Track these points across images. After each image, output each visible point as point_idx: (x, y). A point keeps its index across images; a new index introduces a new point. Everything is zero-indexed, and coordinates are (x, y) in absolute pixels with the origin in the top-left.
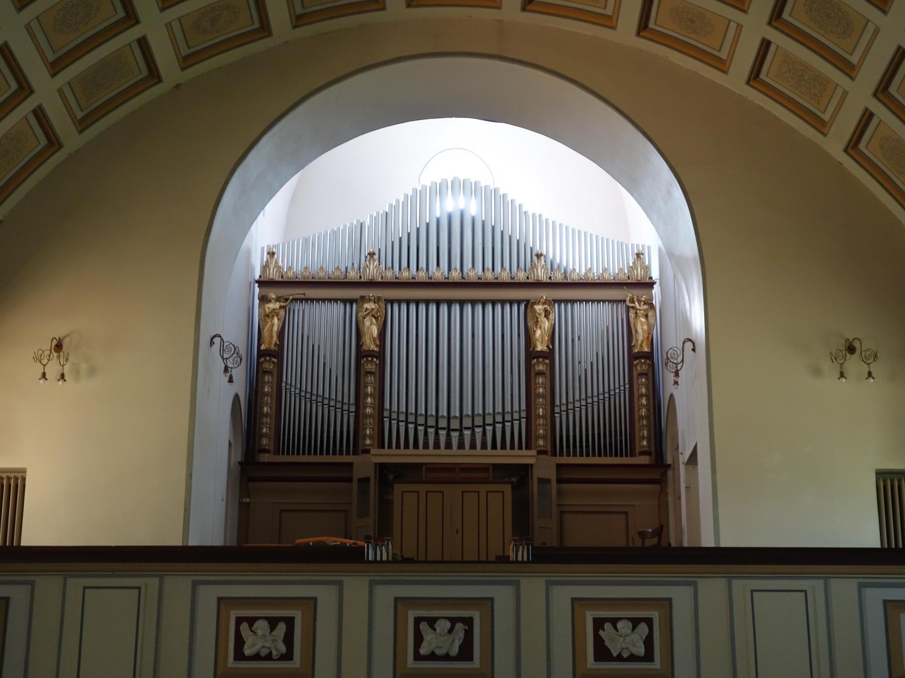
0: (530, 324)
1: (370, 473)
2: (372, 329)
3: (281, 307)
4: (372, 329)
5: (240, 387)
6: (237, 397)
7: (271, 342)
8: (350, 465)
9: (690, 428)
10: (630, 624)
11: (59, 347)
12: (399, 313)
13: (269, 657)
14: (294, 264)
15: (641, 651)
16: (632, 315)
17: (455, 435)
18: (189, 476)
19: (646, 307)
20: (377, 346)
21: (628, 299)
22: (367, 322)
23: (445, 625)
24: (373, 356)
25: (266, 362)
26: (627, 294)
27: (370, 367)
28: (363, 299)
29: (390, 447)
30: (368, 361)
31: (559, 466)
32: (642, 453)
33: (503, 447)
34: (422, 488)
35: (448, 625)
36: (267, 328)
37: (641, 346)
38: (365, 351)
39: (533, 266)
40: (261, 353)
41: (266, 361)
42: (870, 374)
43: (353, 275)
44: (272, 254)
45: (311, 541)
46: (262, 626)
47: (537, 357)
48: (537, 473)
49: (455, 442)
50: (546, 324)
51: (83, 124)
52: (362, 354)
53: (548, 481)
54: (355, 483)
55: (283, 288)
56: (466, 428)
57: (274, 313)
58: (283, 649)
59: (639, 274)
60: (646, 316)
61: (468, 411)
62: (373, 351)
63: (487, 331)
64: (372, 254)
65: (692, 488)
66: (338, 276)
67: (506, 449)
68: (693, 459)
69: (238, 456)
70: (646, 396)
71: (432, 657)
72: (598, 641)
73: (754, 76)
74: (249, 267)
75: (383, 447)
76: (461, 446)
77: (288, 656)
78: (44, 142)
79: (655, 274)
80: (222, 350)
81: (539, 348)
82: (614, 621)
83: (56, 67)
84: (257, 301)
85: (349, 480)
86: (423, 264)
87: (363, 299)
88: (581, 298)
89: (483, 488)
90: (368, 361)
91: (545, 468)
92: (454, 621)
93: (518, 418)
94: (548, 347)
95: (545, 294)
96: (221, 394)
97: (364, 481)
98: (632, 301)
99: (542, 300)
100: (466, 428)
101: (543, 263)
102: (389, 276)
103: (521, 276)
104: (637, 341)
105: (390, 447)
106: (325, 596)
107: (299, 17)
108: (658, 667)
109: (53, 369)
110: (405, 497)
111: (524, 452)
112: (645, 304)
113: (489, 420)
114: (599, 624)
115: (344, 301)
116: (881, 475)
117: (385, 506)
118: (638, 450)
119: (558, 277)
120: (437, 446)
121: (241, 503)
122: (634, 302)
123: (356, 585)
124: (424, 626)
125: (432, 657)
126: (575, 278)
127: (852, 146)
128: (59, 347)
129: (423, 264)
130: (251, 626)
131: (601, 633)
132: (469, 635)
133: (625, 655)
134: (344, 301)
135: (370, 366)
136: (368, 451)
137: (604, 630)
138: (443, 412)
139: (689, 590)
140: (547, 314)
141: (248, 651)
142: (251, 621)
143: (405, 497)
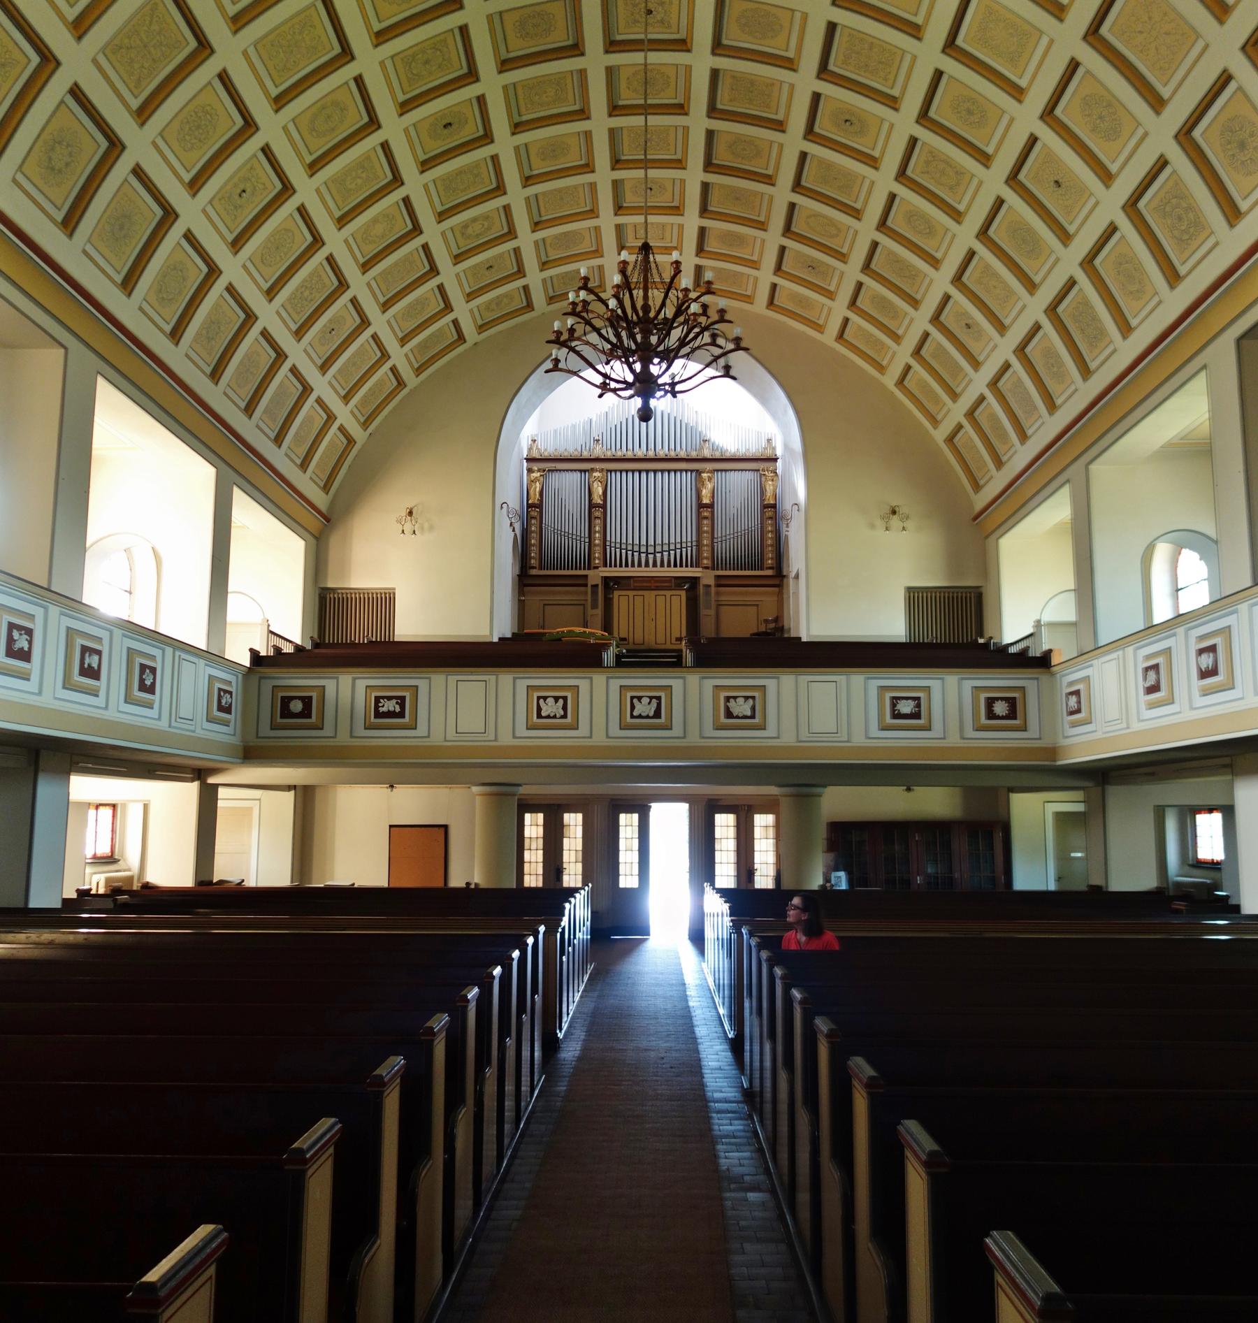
1: (599, 582)
7: (534, 499)
8: (586, 576)
9: (796, 561)
11: (410, 513)
12: (615, 478)
13: (555, 717)
14: (548, 447)
15: (749, 713)
17: (651, 557)
18: (492, 592)
22: (595, 485)
25: (533, 510)
26: (761, 466)
27: (597, 514)
28: (593, 470)
30: (596, 510)
31: (718, 577)
34: (631, 593)
40: (529, 506)
43: (586, 454)
45: (565, 629)
46: (550, 700)
48: (704, 581)
50: (709, 486)
51: (419, 371)
52: (592, 506)
55: (543, 463)
59: (769, 453)
61: (659, 541)
63: (678, 485)
65: (796, 594)
68: (797, 577)
71: (640, 716)
73: (841, 336)
74: (521, 449)
77: (565, 716)
78: (395, 383)
79: (779, 453)
85: (586, 585)
86: (630, 446)
87: (593, 470)
89: (668, 593)
90: (596, 510)
92: (651, 698)
102: (609, 454)
103: (694, 455)
106: (583, 685)
107: (551, 298)
109: (408, 527)
110: (621, 599)
113: (672, 547)
114: (728, 699)
115: (581, 471)
116: (910, 590)
117: (608, 603)
119: (718, 455)
121: (520, 601)
123: (599, 678)
124: (635, 701)
125: (640, 716)
126: (728, 455)
127: (901, 382)
128: (410, 513)
129: (630, 446)
134: (581, 471)
138: (644, 542)
140: (710, 479)
141: (543, 714)
142: (545, 698)
143: (621, 599)
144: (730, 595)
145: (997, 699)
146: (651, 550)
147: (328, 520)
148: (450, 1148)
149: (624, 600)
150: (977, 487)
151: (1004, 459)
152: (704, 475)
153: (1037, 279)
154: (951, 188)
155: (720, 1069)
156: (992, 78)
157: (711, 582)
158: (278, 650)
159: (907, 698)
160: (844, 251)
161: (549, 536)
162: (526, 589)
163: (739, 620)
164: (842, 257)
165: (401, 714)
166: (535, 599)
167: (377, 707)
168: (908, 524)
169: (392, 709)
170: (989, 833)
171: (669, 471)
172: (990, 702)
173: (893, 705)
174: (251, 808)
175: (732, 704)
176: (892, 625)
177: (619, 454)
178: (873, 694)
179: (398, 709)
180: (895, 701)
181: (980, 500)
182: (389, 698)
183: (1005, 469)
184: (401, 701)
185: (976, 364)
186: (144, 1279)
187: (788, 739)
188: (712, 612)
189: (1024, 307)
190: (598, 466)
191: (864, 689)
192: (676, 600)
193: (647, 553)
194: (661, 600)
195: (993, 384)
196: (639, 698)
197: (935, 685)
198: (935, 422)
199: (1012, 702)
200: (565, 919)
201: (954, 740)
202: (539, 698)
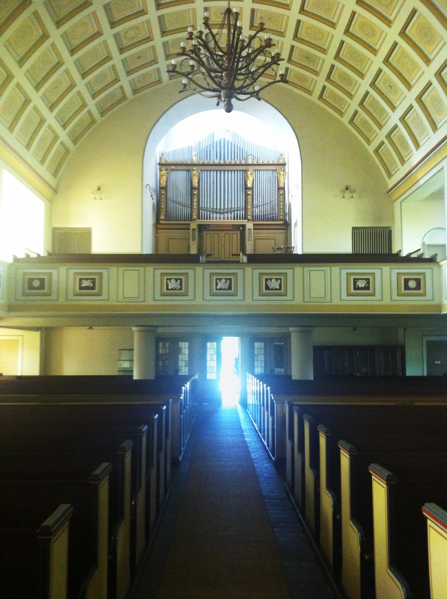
4: (195, 181)
5: (155, 201)
6: (154, 203)
8: (189, 224)
10: (275, 280)
11: (99, 189)
12: (204, 174)
13: (175, 289)
15: (278, 287)
16: (279, 175)
23: (223, 281)
25: (162, 192)
30: (193, 190)
33: (237, 219)
35: (225, 280)
39: (247, 159)
42: (352, 197)
44: (162, 155)
52: (192, 188)
53: (251, 229)
54: (191, 231)
58: (180, 287)
59: (281, 162)
63: (232, 179)
68: (296, 224)
69: (155, 222)
70: (282, 215)
71: (221, 289)
72: (266, 285)
73: (321, 97)
74: (156, 159)
77: (181, 289)
79: (286, 162)
80: (150, 189)
82: (271, 279)
84: (158, 171)
85: (189, 229)
88: (264, 169)
89: (231, 232)
90: (193, 190)
92: (226, 279)
95: (251, 168)
96: (149, 203)
97: (194, 229)
98: (279, 170)
106: (191, 273)
109: (98, 196)
111: (244, 220)
114: (267, 280)
115: (186, 170)
116: (354, 228)
117: (201, 238)
123: (199, 270)
124: (218, 281)
127: (351, 121)
128: (99, 189)
133: (274, 288)
136: (195, 220)
139: (292, 270)
141: (170, 288)
142: (170, 279)
145: (411, 279)
147: (56, 192)
148: (112, 551)
150: (390, 175)
151: (406, 159)
153: (431, 57)
154: (387, 7)
155: (270, 478)
156: (372, 11)
158: (28, 256)
159: (362, 279)
160: (326, 47)
161: (170, 204)
163: (267, 243)
164: (324, 51)
165: (93, 288)
166: (163, 234)
167: (80, 284)
168: (354, 195)
169: (88, 285)
170: (396, 353)
171: (231, 171)
172: (406, 281)
173: (355, 283)
174: (18, 340)
175: (269, 282)
176: (346, 246)
177: (206, 162)
178: (344, 277)
179: (92, 285)
181: (391, 183)
182: (87, 279)
183: (406, 165)
185: (393, 108)
186: (122, 446)
187: (298, 300)
188: (252, 243)
189: (423, 73)
191: (339, 274)
192: (235, 236)
194: (227, 236)
195: (402, 119)
196: (220, 280)
197: (377, 272)
198: (369, 142)
199: (418, 281)
200: (183, 395)
201: (387, 301)
202: (167, 279)
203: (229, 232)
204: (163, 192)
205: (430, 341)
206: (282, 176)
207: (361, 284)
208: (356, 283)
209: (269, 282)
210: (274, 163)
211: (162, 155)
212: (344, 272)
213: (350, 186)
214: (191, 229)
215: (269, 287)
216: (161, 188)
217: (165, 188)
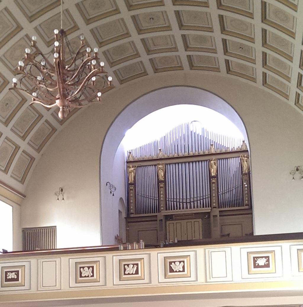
0: (210, 167)
2: (162, 174)
3: (134, 169)
12: (139, 169)
13: (88, 276)
15: (181, 270)
16: (242, 161)
19: (246, 158)
20: (163, 179)
21: (241, 156)
24: (162, 182)
25: (131, 186)
27: (162, 185)
29: (169, 210)
30: (162, 183)
32: (246, 205)
34: (175, 222)
36: (130, 176)
37: (245, 171)
38: (160, 181)
41: (130, 186)
43: (155, 157)
47: (212, 178)
49: (189, 207)
52: (159, 182)
53: (216, 216)
55: (135, 163)
56: (192, 202)
57: (132, 171)
58: (92, 274)
60: (247, 161)
62: (162, 180)
63: (198, 170)
64: (160, 150)
66: (150, 158)
67: (204, 207)
72: (170, 267)
75: (167, 210)
76: (191, 208)
77: (93, 276)
81: (213, 175)
82: (174, 262)
83: (24, 138)
89: (193, 221)
90: (162, 183)
91: (216, 212)
92: (134, 265)
93: (202, 198)
94: (216, 174)
95: (214, 157)
99: (213, 160)
100: (192, 202)
101: (214, 147)
102: (166, 156)
103: (207, 153)
104: (244, 170)
105: (169, 210)
108: (169, 274)
112: (246, 157)
118: (245, 204)
119: (224, 151)
120: (183, 208)
121: (126, 230)
122: (242, 157)
124: (126, 266)
125: (129, 274)
128: (62, 190)
130: (83, 268)
131: (171, 265)
132: (137, 268)
133: (178, 271)
135: (162, 185)
137: (172, 264)
141: (83, 275)
142: (83, 268)
144: (228, 220)
146: (188, 201)
149: (171, 225)
152: (212, 162)
157: (218, 214)
159: (262, 257)
161: (139, 198)
162: (129, 224)
167: (6, 276)
169: (13, 277)
173: (255, 261)
179: (16, 277)
180: (255, 259)
182: (12, 272)
184: (17, 273)
190: (160, 162)
193: (180, 202)
196: (128, 265)
203: (190, 220)
204: (132, 188)
205: (17, 281)
206: (246, 163)
207: (261, 262)
208: (256, 261)
209: (173, 266)
210: (217, 153)
211: (130, 153)
212: (244, 252)
213: (299, 166)
214: (158, 221)
215: (173, 270)
216: (129, 184)
217: (134, 184)
